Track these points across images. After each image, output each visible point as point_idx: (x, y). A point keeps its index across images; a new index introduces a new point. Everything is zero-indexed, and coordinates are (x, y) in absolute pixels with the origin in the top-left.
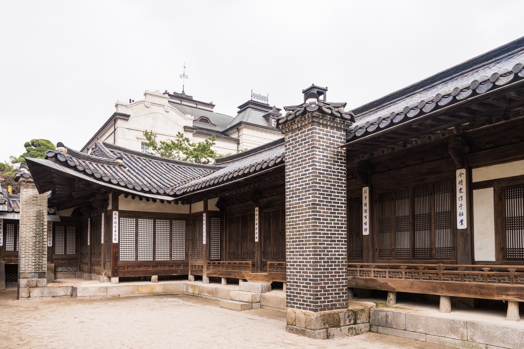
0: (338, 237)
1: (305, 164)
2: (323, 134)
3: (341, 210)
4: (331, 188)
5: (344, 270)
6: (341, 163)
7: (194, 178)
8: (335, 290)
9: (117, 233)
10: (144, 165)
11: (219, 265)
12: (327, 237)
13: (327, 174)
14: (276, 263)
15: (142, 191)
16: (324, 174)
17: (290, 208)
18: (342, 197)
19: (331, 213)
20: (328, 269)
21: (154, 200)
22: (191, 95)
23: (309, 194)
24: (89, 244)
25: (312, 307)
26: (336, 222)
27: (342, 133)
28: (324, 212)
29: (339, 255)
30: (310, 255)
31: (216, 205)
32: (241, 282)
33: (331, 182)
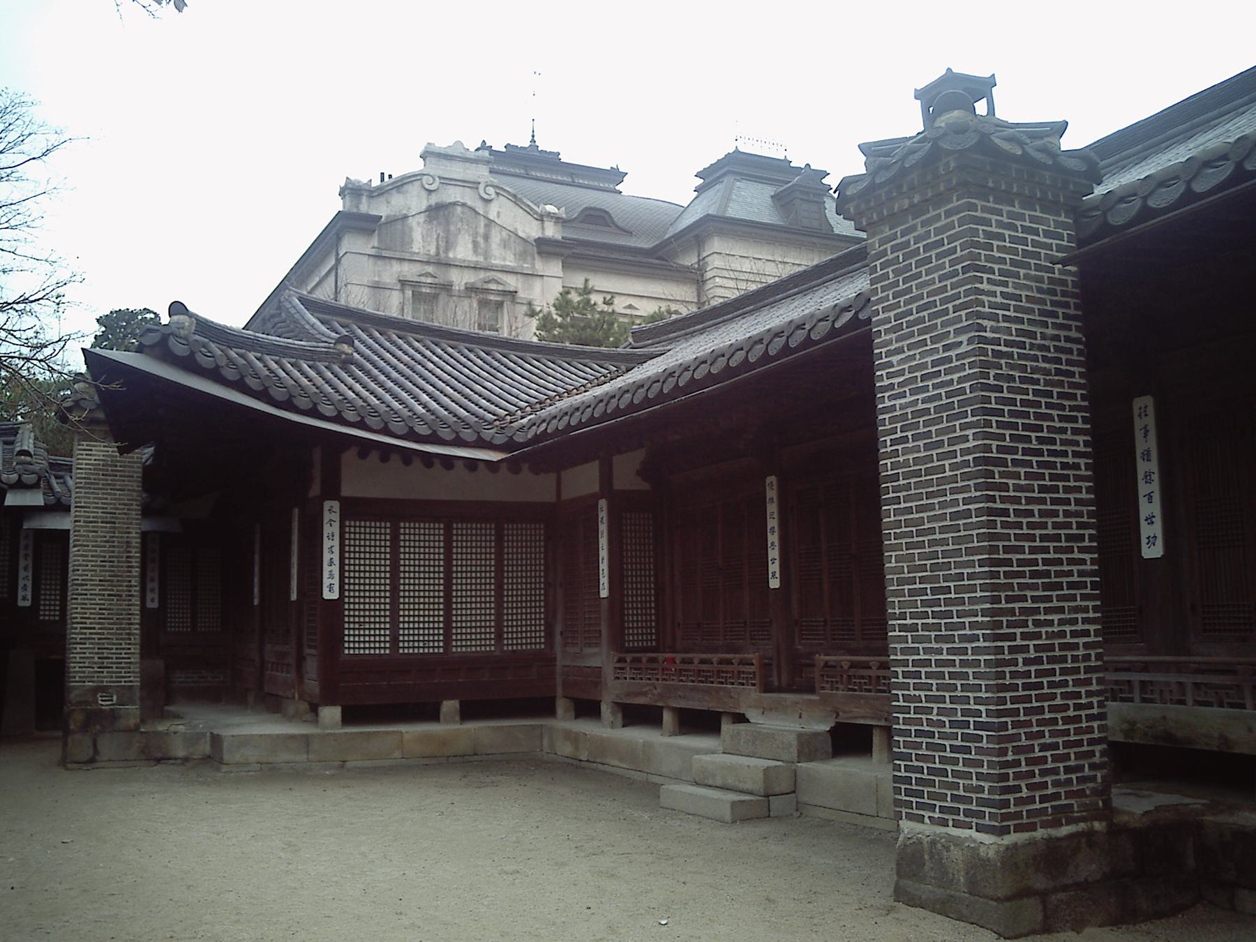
0: (1070, 573)
1: (943, 325)
2: (1000, 224)
3: (1077, 478)
4: (1038, 405)
5: (1094, 687)
6: (1066, 316)
7: (568, 392)
8: (1066, 757)
9: (336, 570)
10: (419, 356)
11: (654, 665)
12: (1034, 575)
13: (1020, 356)
14: (845, 659)
15: (412, 435)
16: (1010, 355)
17: (896, 478)
18: (1075, 431)
19: (1043, 489)
20: (1039, 686)
21: (448, 461)
22: (555, 151)
23: (964, 427)
24: (256, 602)
25: (987, 821)
26: (1061, 519)
27: (1062, 219)
28: (1018, 488)
29: (1074, 634)
30: (975, 638)
31: (638, 473)
32: (727, 727)
33: (1037, 382)
